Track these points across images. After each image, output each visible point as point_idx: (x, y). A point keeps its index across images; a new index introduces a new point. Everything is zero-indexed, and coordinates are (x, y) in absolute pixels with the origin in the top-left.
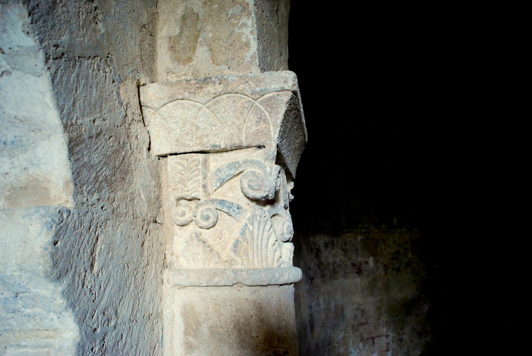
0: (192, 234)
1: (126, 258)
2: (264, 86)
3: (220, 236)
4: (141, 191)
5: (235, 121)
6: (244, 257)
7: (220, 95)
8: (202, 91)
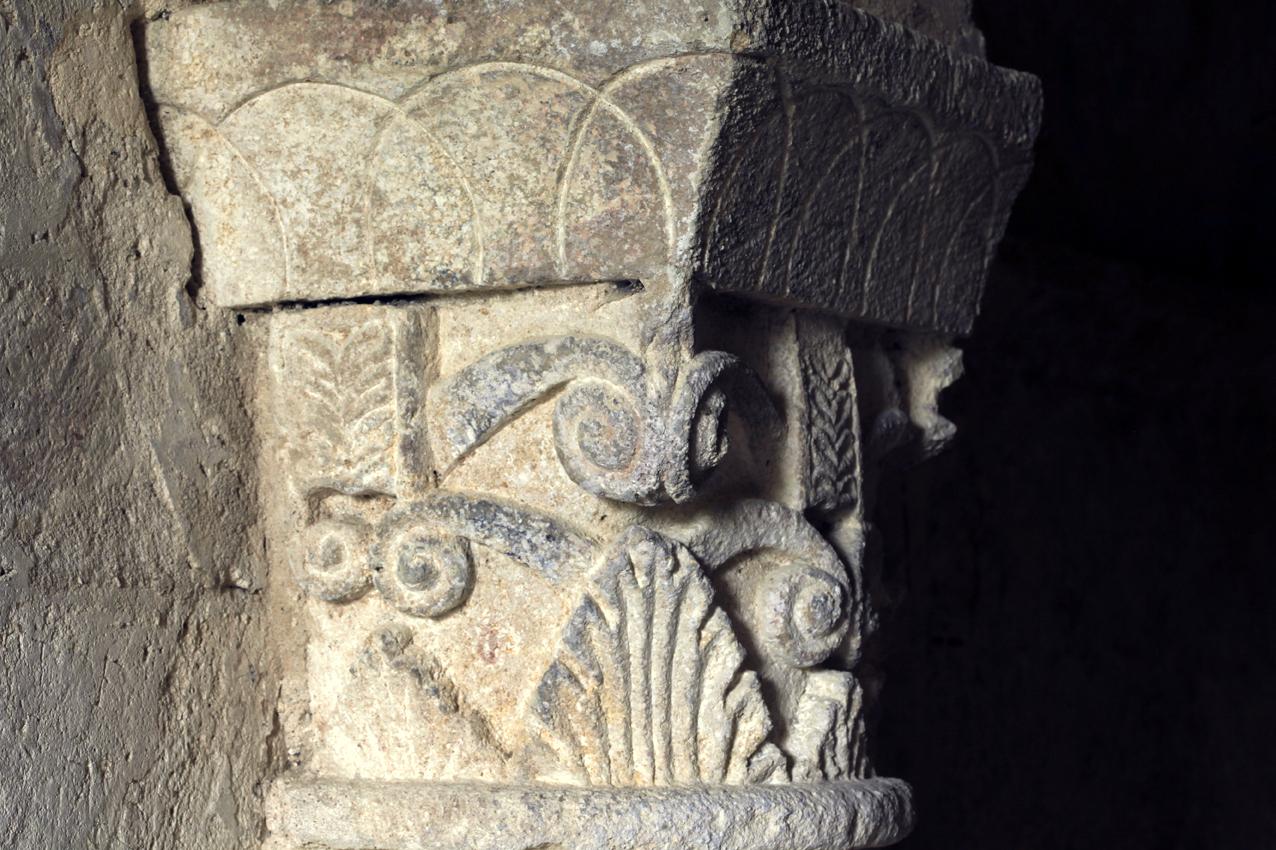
0: (369, 640)
1: (90, 742)
2: (621, 35)
3: (487, 648)
4: (158, 471)
5: (522, 172)
6: (583, 740)
7: (453, 66)
8: (384, 49)
